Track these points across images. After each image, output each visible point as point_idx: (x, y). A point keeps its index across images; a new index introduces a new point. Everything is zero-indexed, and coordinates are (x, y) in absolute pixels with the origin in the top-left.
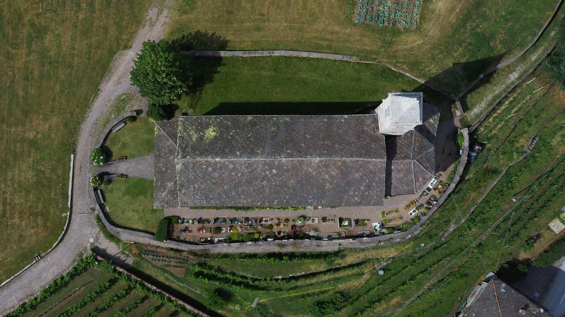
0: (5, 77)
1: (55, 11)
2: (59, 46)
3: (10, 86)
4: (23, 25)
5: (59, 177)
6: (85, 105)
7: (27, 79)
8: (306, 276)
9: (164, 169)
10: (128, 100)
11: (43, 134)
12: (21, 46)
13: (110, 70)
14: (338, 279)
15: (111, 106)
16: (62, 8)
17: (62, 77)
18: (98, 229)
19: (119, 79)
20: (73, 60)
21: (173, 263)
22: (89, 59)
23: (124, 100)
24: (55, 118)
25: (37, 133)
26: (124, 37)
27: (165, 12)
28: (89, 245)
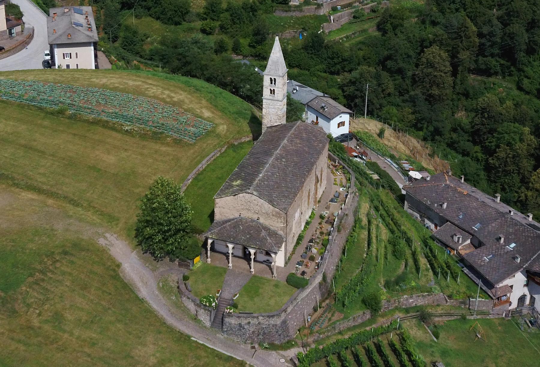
0: (80, 360)
1: (48, 299)
2: (82, 310)
3: (92, 359)
4: (40, 328)
5: (208, 357)
6: (149, 312)
7: (94, 344)
8: (369, 244)
9: (248, 236)
10: (166, 282)
11: (157, 351)
12: (59, 336)
13: (131, 285)
14: (377, 237)
15: (163, 297)
16: (49, 293)
17: (113, 319)
18: (274, 352)
19: (142, 282)
20: (102, 305)
21: (329, 315)
22: (110, 294)
23: (163, 285)
24: (148, 338)
25: (153, 355)
26: (109, 264)
27: (108, 235)
28: (287, 364)
